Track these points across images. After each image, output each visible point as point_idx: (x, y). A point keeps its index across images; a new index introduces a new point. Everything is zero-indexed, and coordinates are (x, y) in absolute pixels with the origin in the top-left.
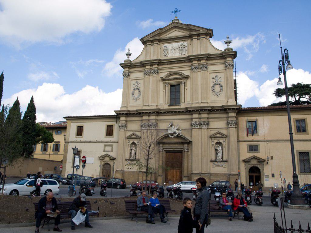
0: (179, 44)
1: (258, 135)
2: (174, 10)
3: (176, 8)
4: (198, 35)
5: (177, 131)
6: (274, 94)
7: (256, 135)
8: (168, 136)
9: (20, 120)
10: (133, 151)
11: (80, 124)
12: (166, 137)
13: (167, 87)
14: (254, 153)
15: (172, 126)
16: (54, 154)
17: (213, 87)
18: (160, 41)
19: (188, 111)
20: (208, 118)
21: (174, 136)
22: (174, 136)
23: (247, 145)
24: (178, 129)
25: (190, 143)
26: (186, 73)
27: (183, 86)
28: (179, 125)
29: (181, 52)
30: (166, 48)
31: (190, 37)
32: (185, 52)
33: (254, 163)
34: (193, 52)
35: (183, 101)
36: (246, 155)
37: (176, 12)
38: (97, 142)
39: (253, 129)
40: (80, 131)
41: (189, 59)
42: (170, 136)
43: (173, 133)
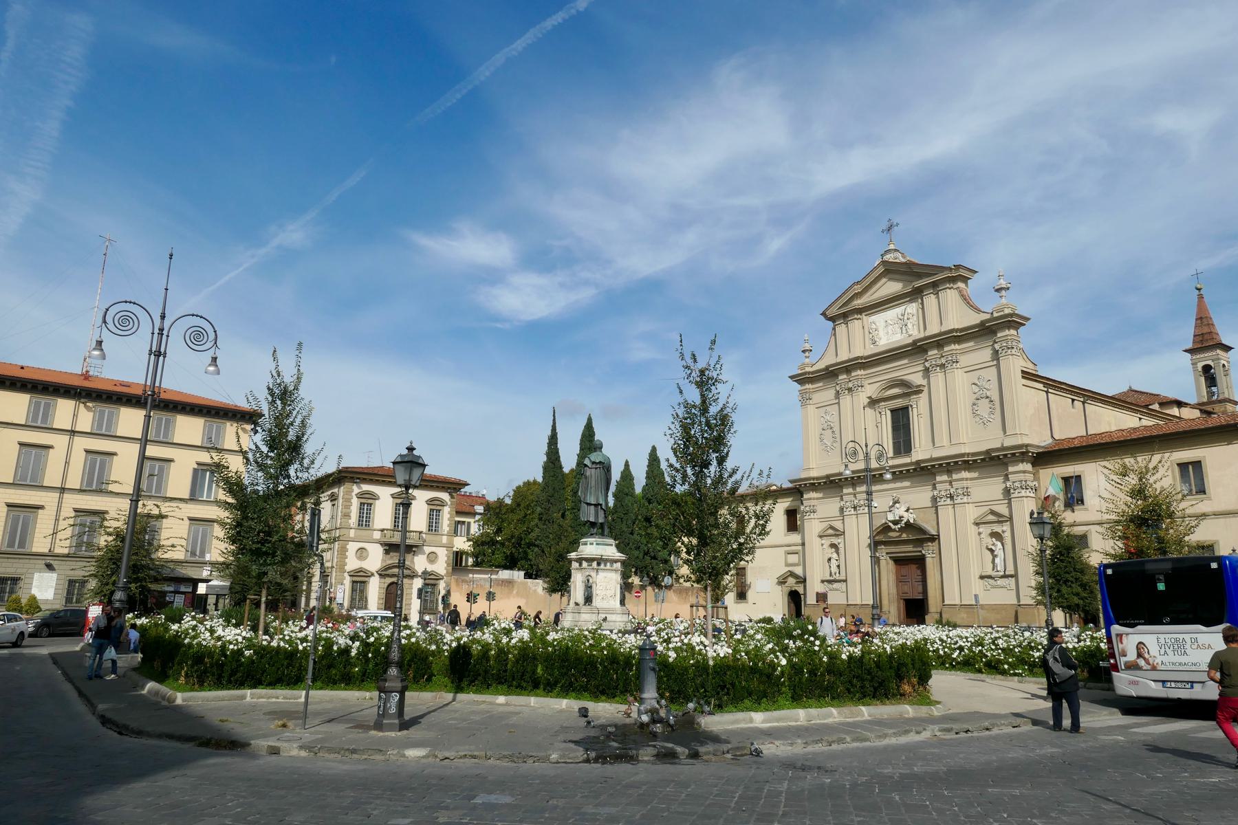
1: (1086, 509)
2: (885, 226)
4: (935, 285)
5: (905, 515)
9: (632, 494)
10: (833, 561)
18: (860, 311)
19: (924, 472)
24: (907, 510)
25: (934, 538)
26: (917, 379)
28: (906, 503)
31: (916, 294)
35: (917, 445)
41: (917, 349)
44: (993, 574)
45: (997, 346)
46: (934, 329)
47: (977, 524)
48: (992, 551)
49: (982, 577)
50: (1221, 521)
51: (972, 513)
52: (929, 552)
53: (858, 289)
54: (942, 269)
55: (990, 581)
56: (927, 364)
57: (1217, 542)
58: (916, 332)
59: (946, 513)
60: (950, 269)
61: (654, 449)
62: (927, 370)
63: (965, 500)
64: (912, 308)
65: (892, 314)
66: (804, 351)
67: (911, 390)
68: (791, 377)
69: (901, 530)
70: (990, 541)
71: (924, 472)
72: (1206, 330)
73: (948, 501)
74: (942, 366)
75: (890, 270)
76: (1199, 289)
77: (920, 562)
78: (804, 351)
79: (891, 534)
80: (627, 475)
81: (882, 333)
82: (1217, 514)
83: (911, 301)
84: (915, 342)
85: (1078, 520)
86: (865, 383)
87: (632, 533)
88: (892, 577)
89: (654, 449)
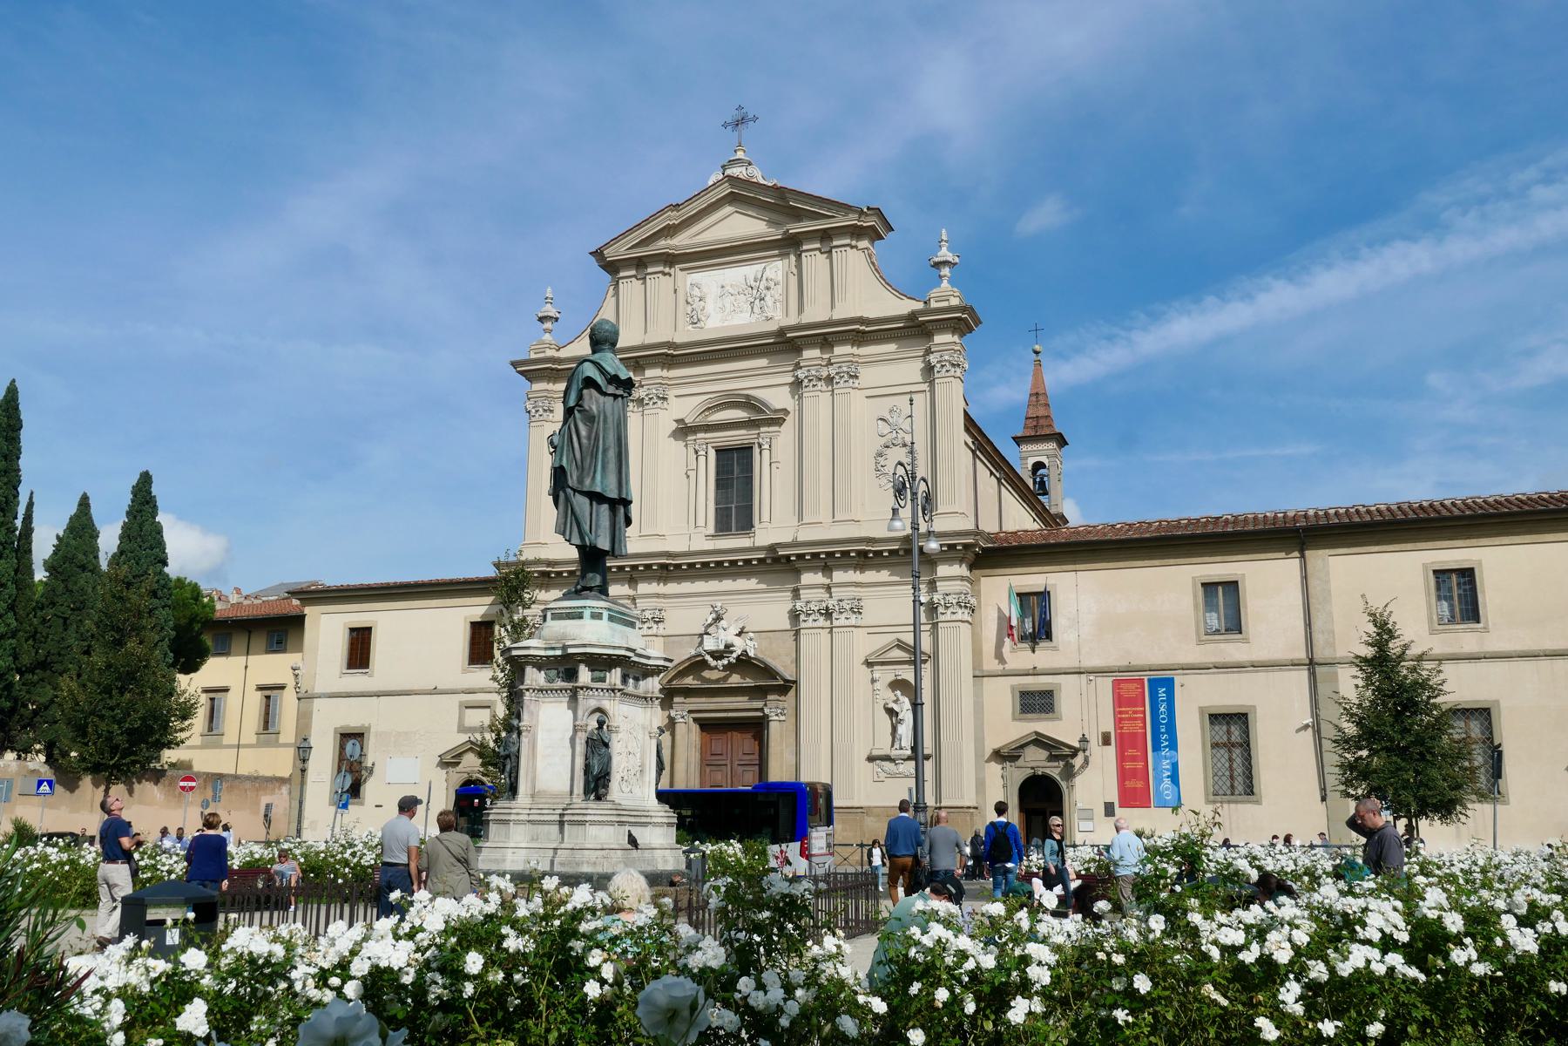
0: (749, 271)
1: (1055, 649)
2: (731, 115)
3: (740, 108)
4: (825, 236)
6: (131, 792)
7: (1047, 648)
8: (703, 664)
9: (95, 569)
11: (359, 615)
12: (697, 665)
13: (702, 459)
14: (1039, 720)
15: (718, 618)
16: (258, 745)
17: (880, 455)
18: (670, 260)
19: (780, 565)
20: (828, 588)
21: (725, 662)
22: (725, 662)
23: (1013, 688)
24: (739, 635)
25: (787, 687)
26: (778, 398)
27: (766, 453)
28: (751, 617)
29: (756, 310)
30: (696, 292)
31: (790, 245)
32: (775, 308)
33: (1036, 759)
34: (801, 310)
35: (766, 517)
36: (1009, 729)
37: (739, 122)
38: (435, 691)
39: (1037, 621)
40: (359, 649)
42: (708, 658)
43: (722, 647)
44: (894, 753)
45: (933, 359)
46: (816, 312)
47: (869, 664)
48: (891, 712)
49: (871, 759)
50: (1261, 676)
51: (866, 644)
52: (774, 708)
53: (674, 218)
54: (846, 208)
55: (887, 764)
56: (801, 374)
57: (1497, 702)
58: (778, 315)
59: (815, 641)
60: (861, 212)
61: (146, 479)
62: (797, 385)
63: (853, 621)
64: (777, 269)
65: (737, 275)
66: (542, 319)
67: (762, 417)
68: (514, 364)
69: (730, 668)
70: (888, 696)
71: (780, 565)
72: (1041, 412)
73: (822, 622)
74: (829, 380)
75: (742, 195)
76: (1037, 353)
77: (757, 727)
78: (542, 319)
79: (706, 674)
80: (82, 527)
81: (710, 306)
82: (1256, 666)
83: (783, 256)
84: (781, 332)
85: (1040, 666)
86: (671, 393)
87: (87, 652)
88: (695, 756)
89: (146, 479)
